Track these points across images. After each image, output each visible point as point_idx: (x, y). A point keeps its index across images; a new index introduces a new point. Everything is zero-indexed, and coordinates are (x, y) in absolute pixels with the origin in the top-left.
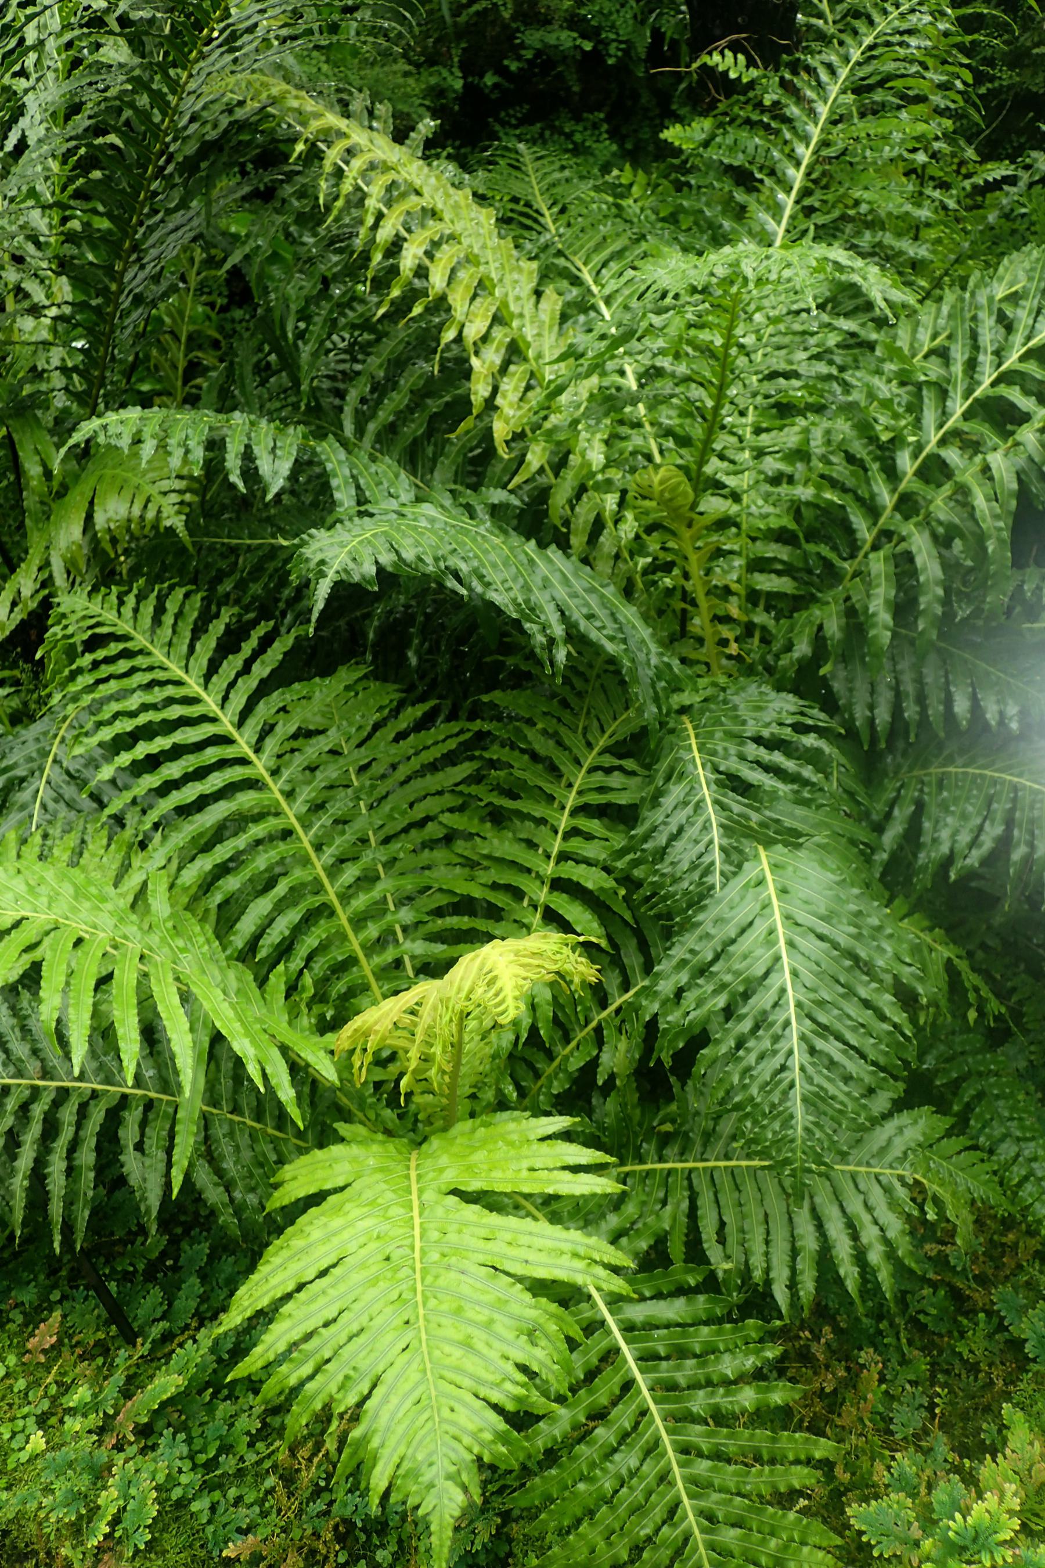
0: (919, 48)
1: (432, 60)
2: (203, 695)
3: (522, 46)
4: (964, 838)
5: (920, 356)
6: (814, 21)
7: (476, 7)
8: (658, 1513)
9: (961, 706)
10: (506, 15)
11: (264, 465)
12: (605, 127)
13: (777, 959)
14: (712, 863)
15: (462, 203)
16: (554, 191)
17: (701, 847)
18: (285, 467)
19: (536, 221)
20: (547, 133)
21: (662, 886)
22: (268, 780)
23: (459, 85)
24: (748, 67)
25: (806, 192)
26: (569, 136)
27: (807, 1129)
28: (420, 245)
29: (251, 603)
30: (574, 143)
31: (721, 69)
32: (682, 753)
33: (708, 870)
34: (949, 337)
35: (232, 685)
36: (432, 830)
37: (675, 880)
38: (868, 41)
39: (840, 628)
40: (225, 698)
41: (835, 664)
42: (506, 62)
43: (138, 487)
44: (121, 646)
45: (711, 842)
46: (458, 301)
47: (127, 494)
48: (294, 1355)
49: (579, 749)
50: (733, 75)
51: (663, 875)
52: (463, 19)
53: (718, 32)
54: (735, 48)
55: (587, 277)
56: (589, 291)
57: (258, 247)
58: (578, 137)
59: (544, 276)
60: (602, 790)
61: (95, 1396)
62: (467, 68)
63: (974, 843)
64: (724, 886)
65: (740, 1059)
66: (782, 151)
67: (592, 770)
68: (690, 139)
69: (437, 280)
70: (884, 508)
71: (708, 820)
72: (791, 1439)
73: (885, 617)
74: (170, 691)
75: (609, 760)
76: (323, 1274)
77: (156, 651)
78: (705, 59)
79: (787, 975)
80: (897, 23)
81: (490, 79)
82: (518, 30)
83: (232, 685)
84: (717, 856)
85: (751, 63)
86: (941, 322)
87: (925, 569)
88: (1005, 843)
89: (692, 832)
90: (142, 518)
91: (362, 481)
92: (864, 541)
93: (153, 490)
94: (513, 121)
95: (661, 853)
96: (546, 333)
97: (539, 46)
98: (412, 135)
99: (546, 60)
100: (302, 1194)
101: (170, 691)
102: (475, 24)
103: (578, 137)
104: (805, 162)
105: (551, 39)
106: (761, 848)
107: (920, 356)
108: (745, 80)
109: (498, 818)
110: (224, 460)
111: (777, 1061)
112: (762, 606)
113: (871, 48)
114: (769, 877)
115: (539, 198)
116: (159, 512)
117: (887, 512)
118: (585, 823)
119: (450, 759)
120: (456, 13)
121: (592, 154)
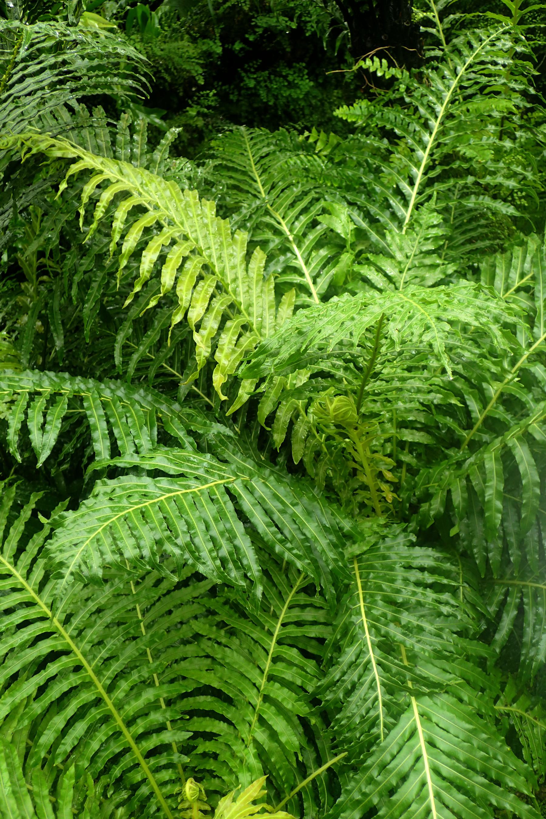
0: (504, 66)
1: (205, 35)
2: (14, 571)
3: (256, 26)
5: (512, 290)
6: (430, 30)
7: (228, 4)
10: (246, 8)
11: (36, 437)
12: (306, 71)
14: (378, 717)
15: (192, 202)
16: (263, 161)
17: (369, 703)
18: (51, 438)
19: (250, 186)
20: (272, 77)
21: (340, 733)
23: (219, 50)
24: (389, 67)
25: (429, 168)
26: (285, 77)
28: (155, 252)
29: (64, 459)
30: (288, 81)
31: (371, 70)
32: (354, 618)
33: (374, 723)
34: (533, 278)
35: (34, 561)
36: (186, 632)
38: (469, 60)
39: (464, 499)
40: (30, 572)
42: (247, 36)
45: (376, 699)
46: (184, 293)
49: (284, 588)
50: (379, 74)
53: (369, 45)
55: (285, 228)
56: (287, 239)
57: (49, 239)
58: (290, 78)
59: (252, 244)
62: (225, 39)
64: (386, 735)
66: (414, 139)
68: (353, 115)
69: (167, 278)
70: (491, 398)
71: (374, 680)
78: (361, 63)
80: (488, 48)
81: (238, 46)
82: (253, 17)
83: (34, 561)
84: (381, 710)
85: (391, 65)
86: (527, 265)
87: (526, 474)
89: (361, 692)
91: (116, 431)
92: (477, 419)
94: (252, 70)
96: (254, 286)
97: (265, 25)
98: (163, 141)
99: (270, 33)
102: (229, 13)
103: (290, 78)
104: (429, 146)
105: (273, 22)
106: (413, 699)
107: (512, 290)
108: (387, 77)
110: (7, 434)
112: (406, 451)
113: (471, 66)
115: (254, 167)
117: (493, 403)
120: (217, 6)
121: (299, 88)
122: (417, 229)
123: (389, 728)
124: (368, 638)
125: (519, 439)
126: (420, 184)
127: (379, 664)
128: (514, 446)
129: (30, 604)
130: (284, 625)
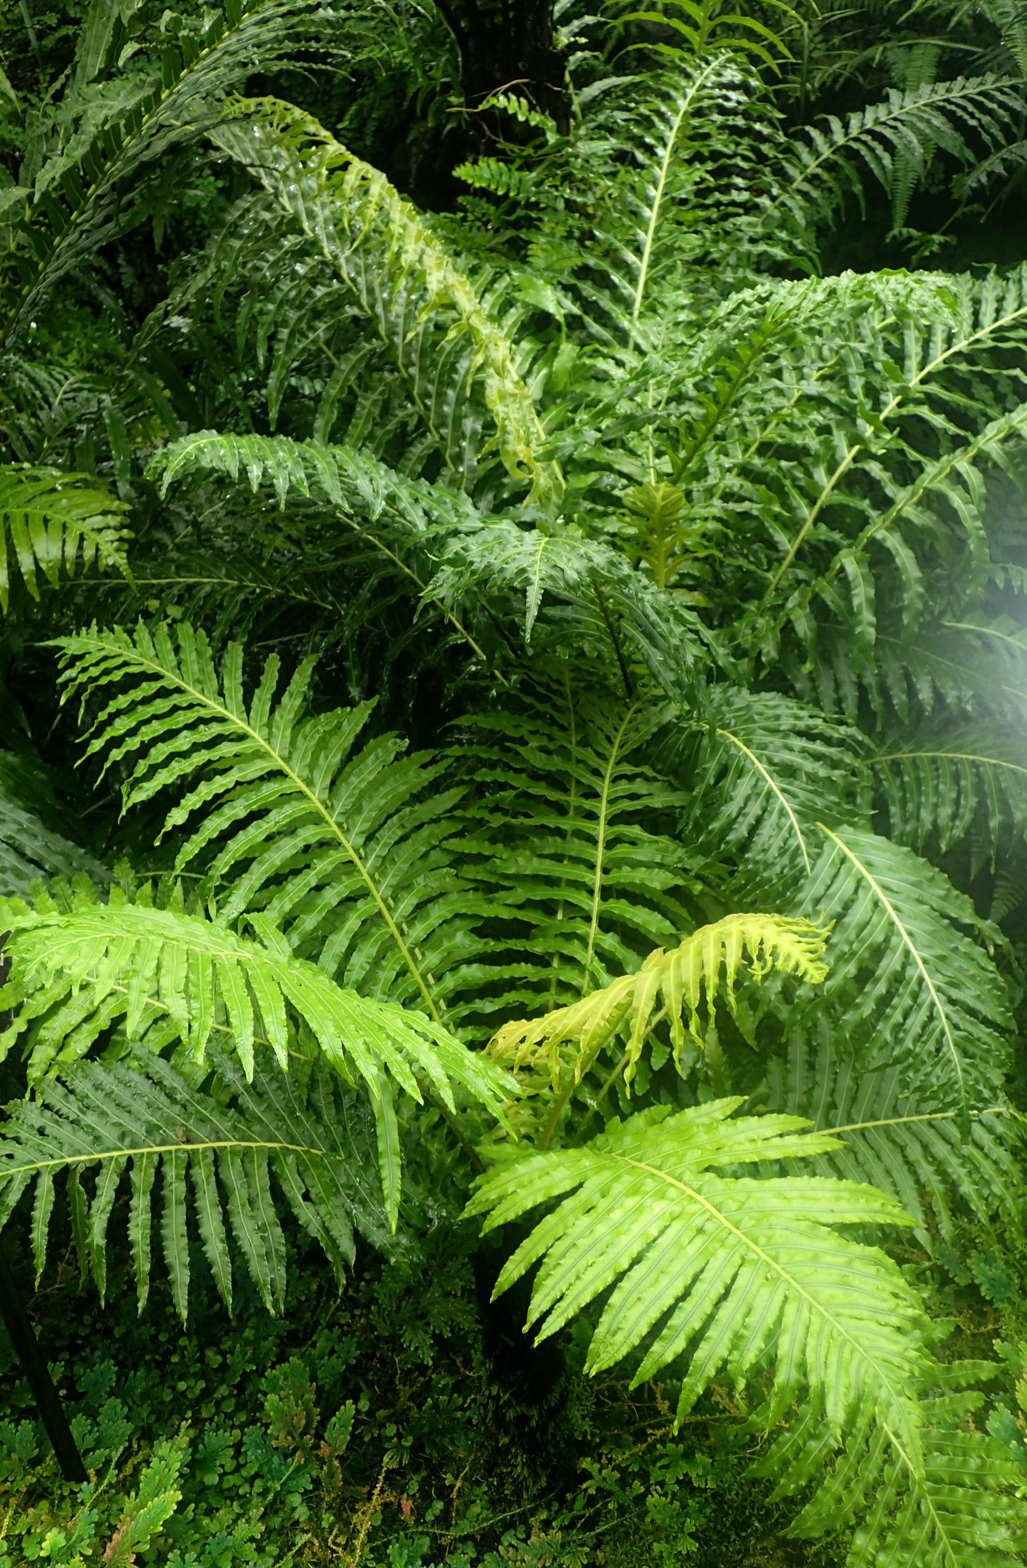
4: (945, 811)
8: (877, 1455)
9: (925, 694)
13: (892, 924)
14: (798, 847)
17: (784, 833)
22: (325, 813)
27: (965, 1071)
33: (796, 852)
37: (768, 866)
41: (815, 662)
43: (64, 527)
44: (156, 686)
47: (55, 530)
48: (665, 1332)
50: (521, 118)
51: (756, 862)
52: (49, 42)
54: (518, 91)
60: (634, 797)
61: (68, 1538)
63: (954, 817)
65: (888, 1018)
67: (614, 780)
70: (805, 520)
72: (961, 1366)
73: (868, 616)
74: (216, 729)
75: (628, 769)
76: (635, 1262)
77: (190, 689)
79: (906, 938)
84: (801, 839)
85: (532, 108)
88: (981, 814)
90: (80, 557)
92: (787, 552)
93: (85, 527)
95: (744, 846)
100: (529, 1205)
101: (216, 729)
109: (509, 837)
111: (923, 1015)
114: (850, 855)
116: (98, 550)
118: (622, 829)
119: (435, 787)
122: (661, 311)
123: (815, 858)
124: (762, 768)
125: (888, 529)
126: (652, 253)
127: (784, 791)
128: (884, 539)
129: (276, 774)
130: (611, 802)
